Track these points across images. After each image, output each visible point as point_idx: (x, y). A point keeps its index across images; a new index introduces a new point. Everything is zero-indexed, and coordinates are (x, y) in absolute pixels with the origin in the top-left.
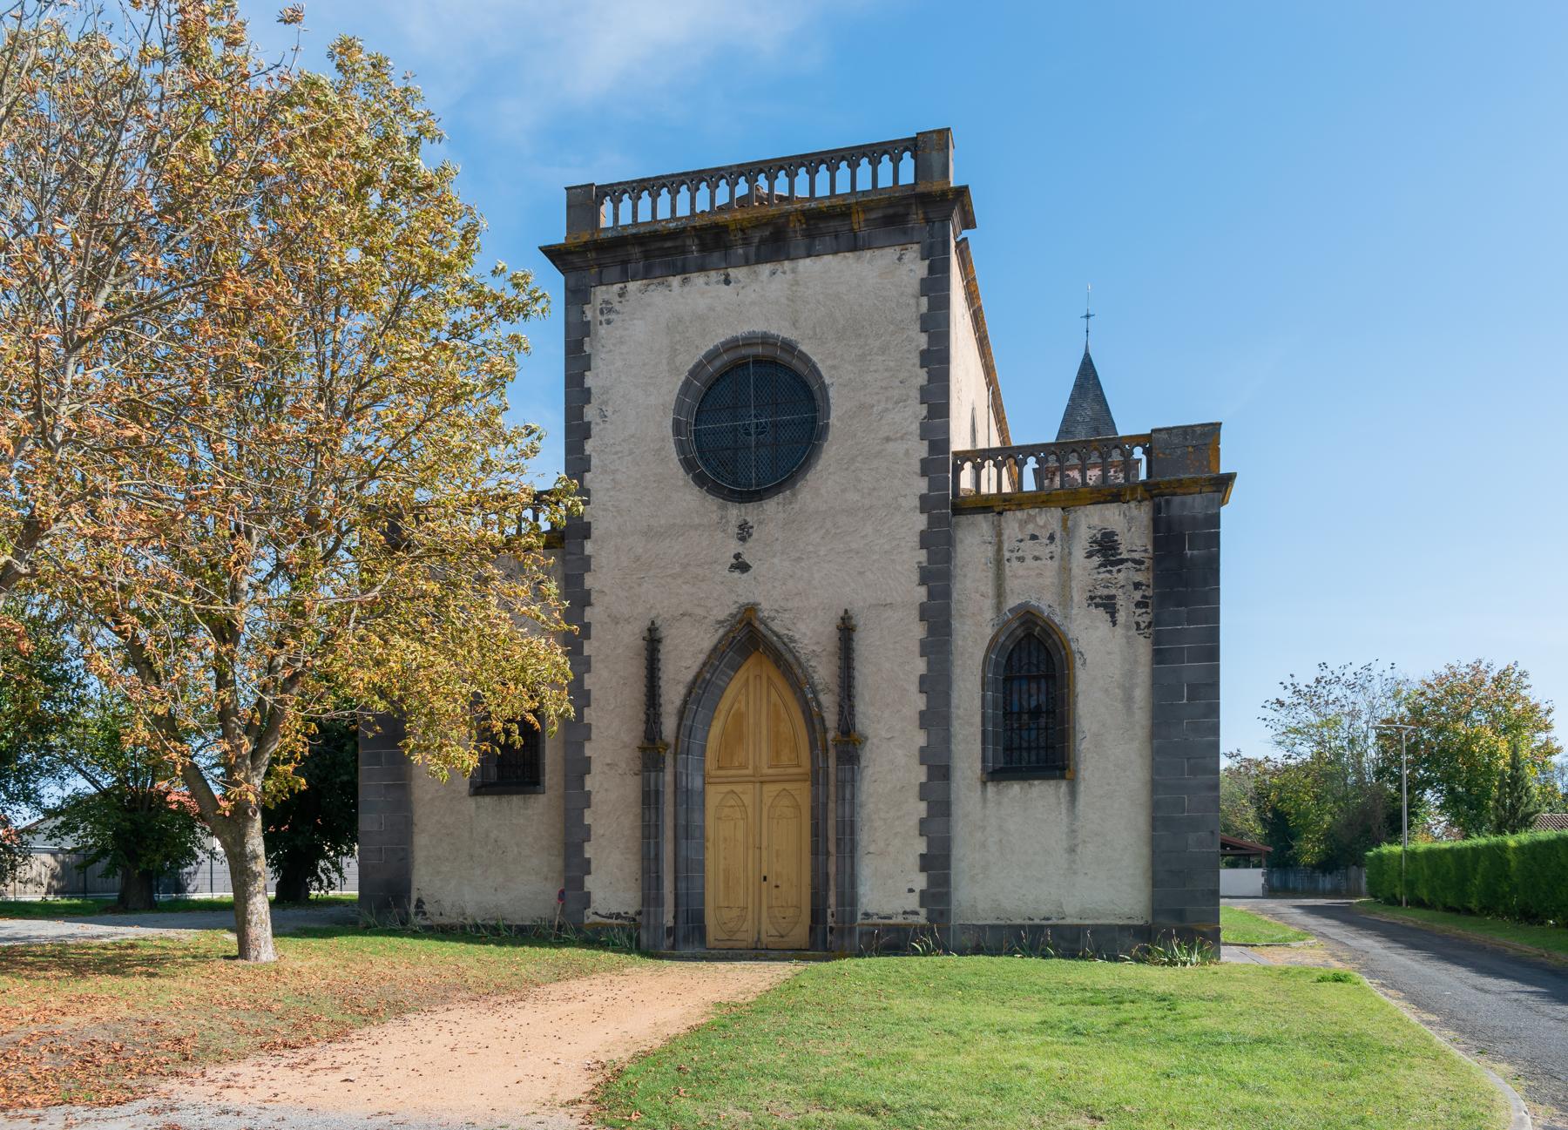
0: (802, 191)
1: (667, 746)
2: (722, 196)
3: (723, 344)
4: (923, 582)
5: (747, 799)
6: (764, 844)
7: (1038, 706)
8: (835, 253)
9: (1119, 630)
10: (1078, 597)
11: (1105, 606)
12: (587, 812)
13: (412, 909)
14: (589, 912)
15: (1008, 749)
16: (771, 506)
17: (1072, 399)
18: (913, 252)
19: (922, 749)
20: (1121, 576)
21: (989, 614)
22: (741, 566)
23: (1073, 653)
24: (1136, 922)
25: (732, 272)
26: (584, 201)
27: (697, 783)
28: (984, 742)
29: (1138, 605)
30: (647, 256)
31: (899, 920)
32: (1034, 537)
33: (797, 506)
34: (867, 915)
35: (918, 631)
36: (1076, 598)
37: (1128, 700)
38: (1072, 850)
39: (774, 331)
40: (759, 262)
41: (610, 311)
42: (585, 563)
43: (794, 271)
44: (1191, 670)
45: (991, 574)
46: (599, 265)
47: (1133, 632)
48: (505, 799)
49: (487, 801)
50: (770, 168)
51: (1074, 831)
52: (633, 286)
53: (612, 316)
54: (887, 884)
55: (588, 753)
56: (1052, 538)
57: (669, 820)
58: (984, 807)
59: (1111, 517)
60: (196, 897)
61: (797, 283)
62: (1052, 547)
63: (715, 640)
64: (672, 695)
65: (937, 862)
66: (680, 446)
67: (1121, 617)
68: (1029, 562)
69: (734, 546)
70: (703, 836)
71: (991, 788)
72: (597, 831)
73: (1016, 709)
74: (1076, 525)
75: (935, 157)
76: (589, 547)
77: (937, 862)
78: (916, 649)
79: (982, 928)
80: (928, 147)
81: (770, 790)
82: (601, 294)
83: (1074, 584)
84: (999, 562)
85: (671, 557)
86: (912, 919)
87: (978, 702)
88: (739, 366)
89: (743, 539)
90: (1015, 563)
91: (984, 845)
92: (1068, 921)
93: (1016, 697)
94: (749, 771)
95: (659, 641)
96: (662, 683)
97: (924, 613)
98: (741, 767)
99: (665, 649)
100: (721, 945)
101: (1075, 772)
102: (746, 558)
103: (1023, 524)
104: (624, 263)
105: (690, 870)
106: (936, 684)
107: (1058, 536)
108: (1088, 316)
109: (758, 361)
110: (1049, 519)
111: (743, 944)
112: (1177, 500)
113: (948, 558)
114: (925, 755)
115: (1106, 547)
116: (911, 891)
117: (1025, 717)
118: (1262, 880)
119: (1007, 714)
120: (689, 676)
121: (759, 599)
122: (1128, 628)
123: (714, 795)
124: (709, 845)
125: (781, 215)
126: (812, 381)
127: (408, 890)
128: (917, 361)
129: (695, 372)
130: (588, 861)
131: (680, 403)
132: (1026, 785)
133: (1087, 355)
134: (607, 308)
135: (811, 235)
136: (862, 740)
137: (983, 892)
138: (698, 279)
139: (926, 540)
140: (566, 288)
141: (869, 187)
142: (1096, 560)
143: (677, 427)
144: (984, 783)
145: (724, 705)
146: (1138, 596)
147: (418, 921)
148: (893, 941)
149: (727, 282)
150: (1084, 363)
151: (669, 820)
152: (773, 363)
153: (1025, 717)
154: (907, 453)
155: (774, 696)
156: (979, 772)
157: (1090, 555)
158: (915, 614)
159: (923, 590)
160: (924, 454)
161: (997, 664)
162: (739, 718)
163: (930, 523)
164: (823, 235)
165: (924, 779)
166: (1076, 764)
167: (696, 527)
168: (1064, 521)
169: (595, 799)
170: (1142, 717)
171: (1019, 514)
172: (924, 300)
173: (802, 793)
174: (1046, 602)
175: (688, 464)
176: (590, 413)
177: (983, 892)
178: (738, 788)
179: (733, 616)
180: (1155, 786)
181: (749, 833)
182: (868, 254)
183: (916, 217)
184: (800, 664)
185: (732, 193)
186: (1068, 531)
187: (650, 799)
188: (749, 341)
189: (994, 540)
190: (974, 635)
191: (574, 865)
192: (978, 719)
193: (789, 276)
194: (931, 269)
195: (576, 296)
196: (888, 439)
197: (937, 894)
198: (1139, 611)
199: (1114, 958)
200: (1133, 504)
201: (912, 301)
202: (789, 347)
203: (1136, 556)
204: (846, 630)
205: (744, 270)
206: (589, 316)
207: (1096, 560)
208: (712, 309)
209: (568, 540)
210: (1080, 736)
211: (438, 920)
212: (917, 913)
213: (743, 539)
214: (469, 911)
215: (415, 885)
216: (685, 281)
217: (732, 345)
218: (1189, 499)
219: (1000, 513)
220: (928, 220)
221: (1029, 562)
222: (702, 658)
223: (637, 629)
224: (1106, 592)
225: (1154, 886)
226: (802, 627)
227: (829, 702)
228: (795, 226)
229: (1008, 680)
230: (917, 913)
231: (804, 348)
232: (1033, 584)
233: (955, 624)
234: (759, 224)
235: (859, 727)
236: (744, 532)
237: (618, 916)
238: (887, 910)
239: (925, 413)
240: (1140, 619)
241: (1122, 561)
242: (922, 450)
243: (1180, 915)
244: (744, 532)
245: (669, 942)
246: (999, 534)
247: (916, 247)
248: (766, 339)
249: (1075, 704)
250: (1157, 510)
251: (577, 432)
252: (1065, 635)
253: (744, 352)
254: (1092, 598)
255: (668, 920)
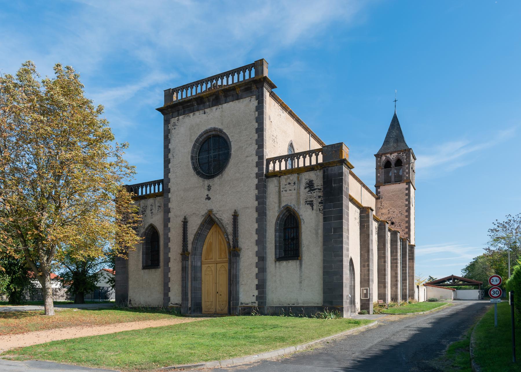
0: (225, 83)
1: (189, 253)
2: (209, 85)
3: (204, 132)
4: (257, 200)
5: (213, 269)
6: (217, 282)
7: (294, 237)
8: (233, 101)
9: (314, 211)
10: (302, 202)
11: (310, 204)
12: (169, 273)
13: (128, 303)
14: (170, 303)
15: (285, 251)
16: (216, 179)
17: (389, 130)
18: (254, 98)
19: (257, 252)
20: (315, 194)
21: (277, 209)
22: (208, 198)
23: (300, 219)
24: (319, 305)
25: (206, 110)
26: (169, 94)
27: (199, 264)
28: (275, 249)
29: (320, 203)
30: (184, 108)
31: (250, 305)
32: (289, 184)
33: (223, 179)
34: (242, 303)
35: (255, 215)
36: (301, 202)
37: (317, 234)
38: (301, 282)
39: (217, 127)
40: (212, 106)
41: (175, 125)
42: (169, 200)
43: (222, 108)
44: (334, 223)
45: (277, 196)
46: (172, 112)
47: (318, 212)
48: (151, 270)
49: (146, 271)
50: (216, 77)
51: (301, 276)
52: (181, 117)
53: (176, 127)
54: (247, 295)
55: (169, 256)
56: (294, 183)
57: (191, 275)
58: (275, 269)
59: (312, 175)
60: (111, 300)
61: (223, 111)
62: (295, 186)
63: (201, 221)
64: (191, 238)
65: (261, 287)
66: (193, 164)
67: (315, 207)
68: (288, 191)
69: (206, 192)
70: (201, 280)
71: (277, 263)
72: (172, 279)
73: (287, 238)
74: (301, 179)
75: (260, 68)
76: (170, 195)
77: (261, 287)
78: (255, 221)
79: (276, 307)
80: (258, 65)
81: (219, 265)
82: (173, 120)
83: (301, 198)
84: (279, 192)
85: (190, 198)
86: (254, 304)
87: (274, 237)
88: (208, 139)
89: (209, 190)
90: (284, 192)
91: (275, 281)
92: (300, 305)
93: (287, 234)
94: (213, 260)
95: (187, 222)
96: (188, 234)
97: (257, 209)
98: (212, 259)
99: (189, 224)
100: (206, 313)
101: (302, 257)
102: (210, 196)
103: (286, 180)
104: (178, 111)
105: (197, 290)
106: (261, 232)
107: (296, 183)
108: (395, 101)
109: (214, 136)
110: (293, 178)
111: (211, 313)
112: (330, 168)
113: (265, 192)
114: (257, 254)
115: (310, 185)
116: (254, 296)
117: (290, 240)
118: (479, 294)
119: (285, 240)
120: (195, 232)
121: (213, 208)
122: (317, 211)
123: (204, 267)
124: (203, 282)
125: (216, 92)
126: (228, 141)
127: (127, 297)
128: (255, 132)
129: (196, 141)
130: (169, 288)
131: (193, 151)
132: (287, 262)
133: (395, 114)
134: (174, 125)
135: (226, 96)
136: (240, 250)
137: (276, 296)
138: (197, 113)
139: (257, 187)
140: (164, 120)
141: (220, 84)
142: (308, 189)
143: (192, 158)
144: (275, 262)
145: (207, 240)
146: (320, 200)
147: (130, 306)
148: (247, 311)
149: (205, 113)
150: (394, 117)
151: (191, 275)
152: (219, 136)
153: (290, 240)
154: (252, 160)
155: (220, 237)
156: (274, 258)
157: (305, 188)
158: (255, 210)
159: (257, 202)
160: (257, 160)
161: (280, 224)
162: (211, 244)
163: (259, 182)
164: (229, 96)
165: (257, 261)
166: (302, 255)
167: (197, 187)
168: (298, 178)
169: (171, 270)
170: (321, 239)
171: (285, 177)
172: (257, 112)
173: (226, 265)
174: (293, 204)
175: (195, 169)
176: (170, 156)
177: (276, 296)
178: (210, 265)
179: (206, 213)
180: (324, 261)
181: (212, 280)
182: (241, 100)
183: (254, 87)
184: (224, 227)
185: (211, 84)
186: (299, 180)
187: (184, 269)
188: (210, 130)
189: (278, 185)
190: (273, 214)
191: (166, 290)
192: (274, 242)
193: (221, 109)
194: (259, 103)
195: (167, 122)
196: (247, 156)
197: (261, 296)
198: (320, 205)
199: (310, 317)
200: (318, 171)
201: (254, 113)
202: (221, 131)
203: (319, 187)
204: (235, 216)
205: (209, 109)
206: (170, 127)
207: (308, 189)
208: (201, 122)
209: (165, 193)
210: (303, 246)
211: (135, 306)
212: (255, 303)
213: (209, 190)
214: (142, 303)
215: (129, 295)
216: (194, 114)
217: (206, 132)
218: (333, 168)
219: (280, 177)
220: (257, 88)
221: (288, 191)
222: (198, 226)
223: (182, 219)
224: (311, 199)
225: (324, 293)
226: (224, 216)
227: (231, 237)
228: (221, 94)
229: (285, 229)
230: (255, 303)
231: (224, 131)
232: (289, 198)
233: (267, 212)
234: (211, 95)
235: (239, 246)
236: (209, 188)
237: (177, 304)
238: (247, 302)
239: (257, 147)
240: (320, 208)
241: (315, 189)
242: (256, 159)
243: (331, 303)
244: (209, 188)
245: (189, 312)
246: (280, 183)
247: (255, 96)
248: (215, 129)
249: (301, 236)
250: (324, 172)
251: (167, 162)
252: (298, 214)
253: (210, 133)
254: (306, 202)
255: (189, 305)
